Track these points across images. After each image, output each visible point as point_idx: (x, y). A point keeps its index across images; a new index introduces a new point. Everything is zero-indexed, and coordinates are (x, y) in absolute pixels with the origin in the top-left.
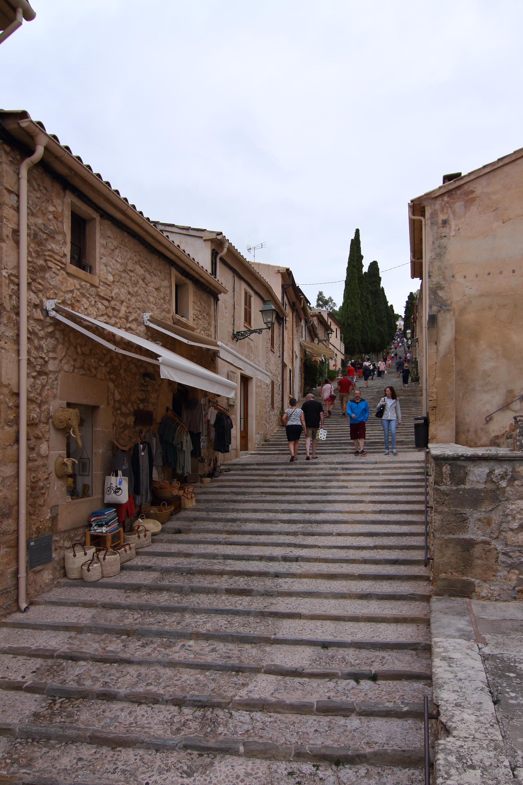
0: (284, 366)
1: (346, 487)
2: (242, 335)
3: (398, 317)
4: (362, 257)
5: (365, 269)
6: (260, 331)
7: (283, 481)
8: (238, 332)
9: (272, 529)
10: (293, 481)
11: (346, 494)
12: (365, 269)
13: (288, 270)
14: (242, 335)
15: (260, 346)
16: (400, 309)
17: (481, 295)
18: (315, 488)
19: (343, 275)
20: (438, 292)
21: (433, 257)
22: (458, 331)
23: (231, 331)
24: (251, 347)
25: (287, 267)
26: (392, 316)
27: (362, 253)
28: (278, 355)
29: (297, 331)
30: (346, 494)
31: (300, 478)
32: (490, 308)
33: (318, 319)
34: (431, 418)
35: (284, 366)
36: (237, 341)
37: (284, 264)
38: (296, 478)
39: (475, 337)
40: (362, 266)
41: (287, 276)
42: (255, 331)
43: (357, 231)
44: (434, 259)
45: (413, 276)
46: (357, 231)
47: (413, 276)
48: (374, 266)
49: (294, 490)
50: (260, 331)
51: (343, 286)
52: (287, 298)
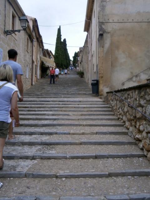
0: (33, 62)
1: (68, 115)
2: (10, 32)
3: (71, 60)
4: (61, 35)
5: (62, 40)
6: (19, 31)
7: (29, 111)
8: (7, 31)
9: (14, 153)
10: (35, 111)
11: (69, 119)
12: (62, 40)
13: (35, 19)
14: (10, 32)
15: (21, 45)
16: (71, 58)
17: (120, 29)
18: (48, 115)
19: (56, 37)
20: (102, 26)
21: (100, 10)
22: (112, 44)
23: (3, 28)
24: (16, 44)
25: (35, 18)
26: (70, 60)
27: (61, 34)
28: (30, 55)
29: (39, 51)
30: (69, 119)
31: (39, 109)
32: (124, 35)
33: (47, 51)
34: (101, 82)
35: (33, 62)
36: (7, 35)
37: (34, 16)
38: (36, 109)
39: (118, 48)
40: (61, 38)
41: (35, 21)
42: (16, 31)
43: (60, 26)
44: (100, 11)
45: (85, 31)
46: (60, 26)
47: (85, 31)
48: (65, 40)
49: (34, 117)
50: (19, 31)
51: (55, 46)
52: (35, 33)
